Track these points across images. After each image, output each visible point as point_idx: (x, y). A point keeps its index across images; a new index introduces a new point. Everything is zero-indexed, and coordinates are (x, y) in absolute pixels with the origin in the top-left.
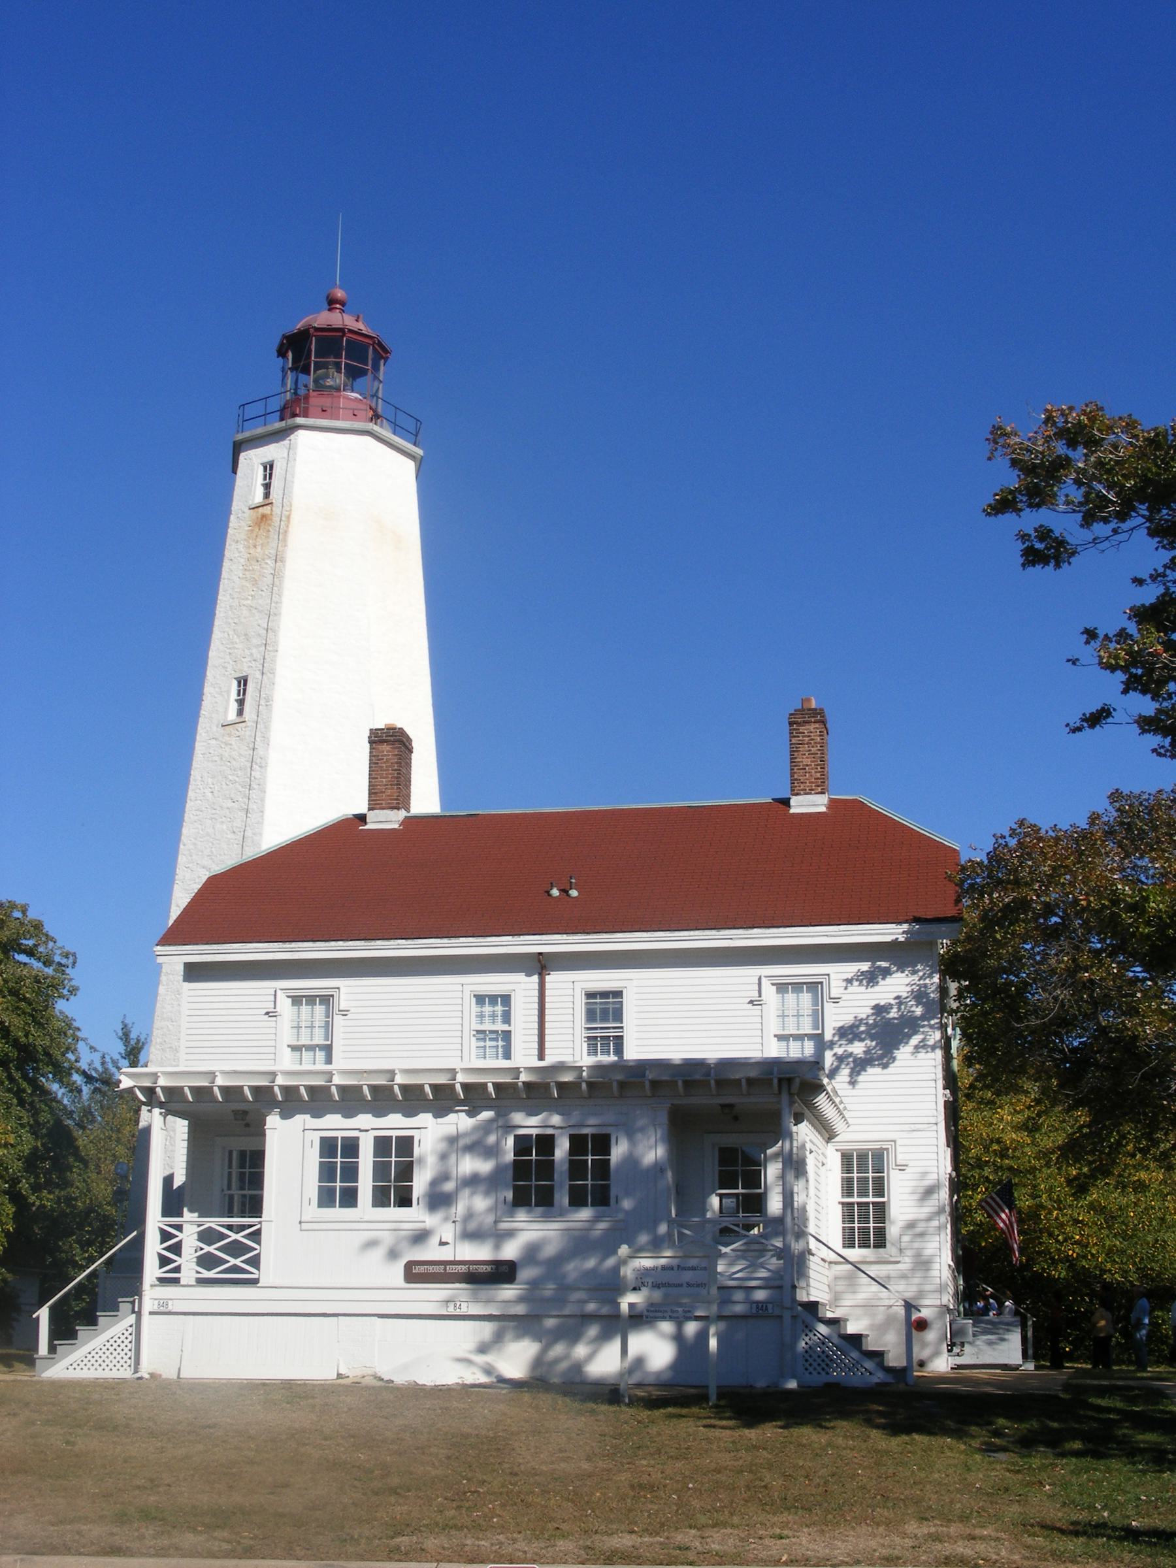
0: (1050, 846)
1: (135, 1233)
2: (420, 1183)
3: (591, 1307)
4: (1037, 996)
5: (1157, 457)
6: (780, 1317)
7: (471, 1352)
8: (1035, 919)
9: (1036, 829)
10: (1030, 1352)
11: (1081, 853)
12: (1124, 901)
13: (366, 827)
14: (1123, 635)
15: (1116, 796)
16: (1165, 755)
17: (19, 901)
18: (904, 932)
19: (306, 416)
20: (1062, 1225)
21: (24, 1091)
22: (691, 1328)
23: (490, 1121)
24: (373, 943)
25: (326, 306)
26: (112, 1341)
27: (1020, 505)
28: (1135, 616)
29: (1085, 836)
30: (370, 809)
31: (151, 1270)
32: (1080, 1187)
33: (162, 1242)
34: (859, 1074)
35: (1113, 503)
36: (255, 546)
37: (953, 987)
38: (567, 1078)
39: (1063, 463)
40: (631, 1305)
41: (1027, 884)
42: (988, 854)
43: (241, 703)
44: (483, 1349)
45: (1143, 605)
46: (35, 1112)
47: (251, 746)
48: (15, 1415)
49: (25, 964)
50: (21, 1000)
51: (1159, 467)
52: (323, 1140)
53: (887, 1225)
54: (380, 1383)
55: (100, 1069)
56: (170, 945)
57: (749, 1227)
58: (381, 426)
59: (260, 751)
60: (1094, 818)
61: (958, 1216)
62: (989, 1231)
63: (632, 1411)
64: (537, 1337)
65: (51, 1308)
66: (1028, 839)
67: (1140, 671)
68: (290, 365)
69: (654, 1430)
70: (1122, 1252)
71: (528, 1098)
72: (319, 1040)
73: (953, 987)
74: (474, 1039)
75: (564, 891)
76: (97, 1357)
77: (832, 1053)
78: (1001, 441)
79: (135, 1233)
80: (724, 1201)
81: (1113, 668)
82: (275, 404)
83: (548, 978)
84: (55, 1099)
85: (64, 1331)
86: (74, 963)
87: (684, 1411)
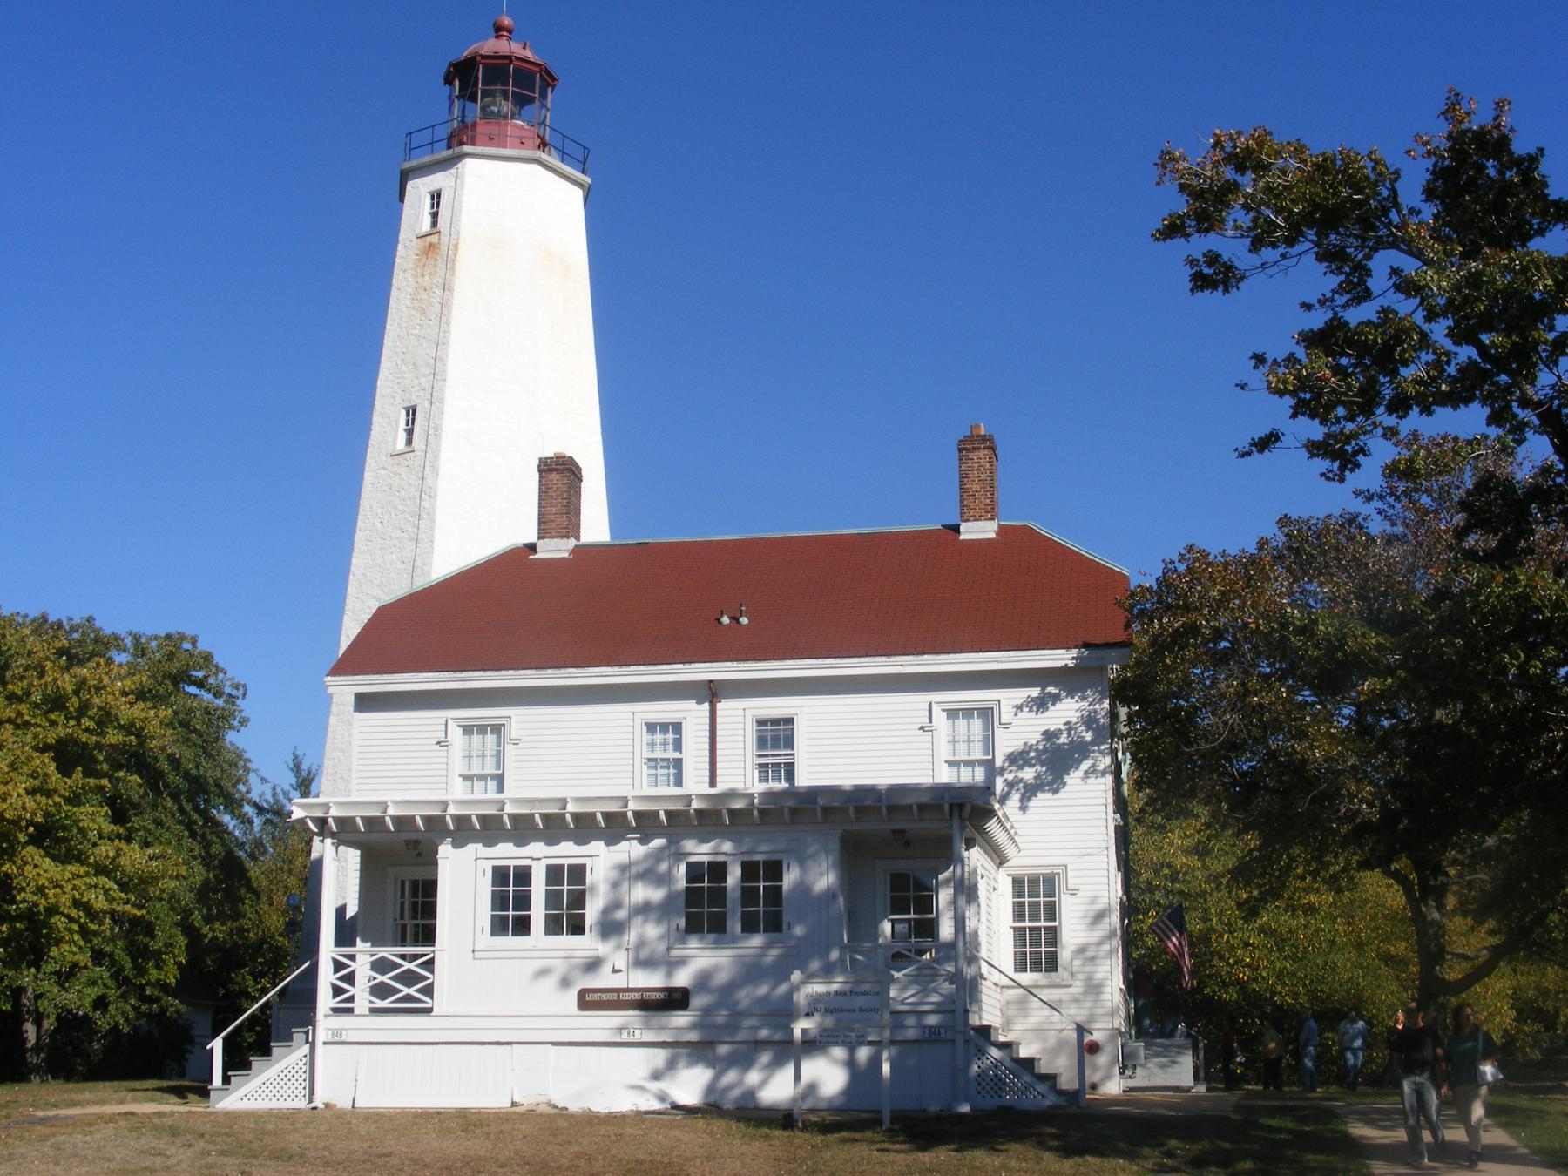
0: (1218, 571)
1: (308, 963)
2: (592, 911)
3: (764, 1033)
4: (1206, 720)
5: (1325, 182)
6: (953, 1041)
7: (644, 1079)
8: (1205, 643)
9: (1204, 554)
10: (1202, 1074)
11: (1250, 578)
12: (1293, 624)
13: (536, 556)
14: (1291, 359)
15: (1284, 521)
16: (1334, 480)
17: (189, 632)
18: (1073, 658)
19: (473, 143)
20: (1233, 948)
21: (195, 823)
22: (863, 1053)
23: (662, 849)
24: (543, 672)
25: (493, 33)
26: (286, 1072)
27: (1188, 230)
28: (1303, 341)
29: (1253, 560)
30: (539, 538)
31: (325, 1000)
32: (1250, 911)
33: (336, 971)
34: (1029, 799)
35: (1281, 228)
36: (423, 276)
37: (1123, 712)
38: (738, 805)
39: (1232, 188)
40: (804, 1031)
41: (1196, 609)
42: (1158, 579)
43: (410, 432)
44: (656, 1076)
45: (1312, 330)
46: (207, 845)
47: (420, 476)
48: (190, 1146)
49: (195, 696)
50: (191, 732)
51: (1327, 192)
52: (496, 869)
53: (1059, 949)
54: (553, 1111)
55: (271, 800)
56: (340, 675)
57: (921, 952)
58: (549, 154)
59: (429, 481)
60: (1262, 543)
61: (1130, 940)
62: (1160, 956)
63: (806, 1136)
64: (711, 1063)
65: (225, 1040)
66: (1197, 565)
67: (1308, 396)
68: (457, 93)
69: (828, 1154)
70: (1293, 974)
71: (700, 825)
72: (490, 768)
73: (1123, 712)
74: (645, 767)
75: (735, 619)
76: (271, 1087)
77: (1002, 779)
78: (1170, 166)
79: (308, 963)
80: (896, 926)
81: (1281, 393)
82: (443, 132)
83: (719, 706)
84: (226, 831)
85: (237, 1061)
86: (245, 694)
87: (858, 1135)
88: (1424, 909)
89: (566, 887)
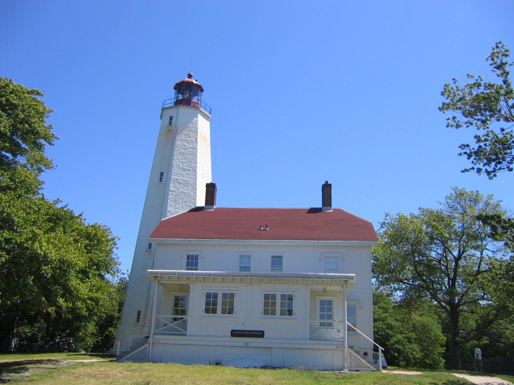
88: (452, 238)
89: (228, 300)
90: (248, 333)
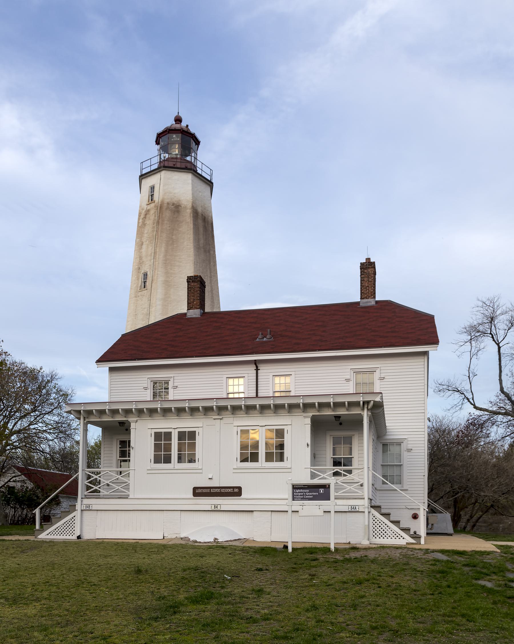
65: (41, 509)
85: (47, 520)
90: (218, 490)
